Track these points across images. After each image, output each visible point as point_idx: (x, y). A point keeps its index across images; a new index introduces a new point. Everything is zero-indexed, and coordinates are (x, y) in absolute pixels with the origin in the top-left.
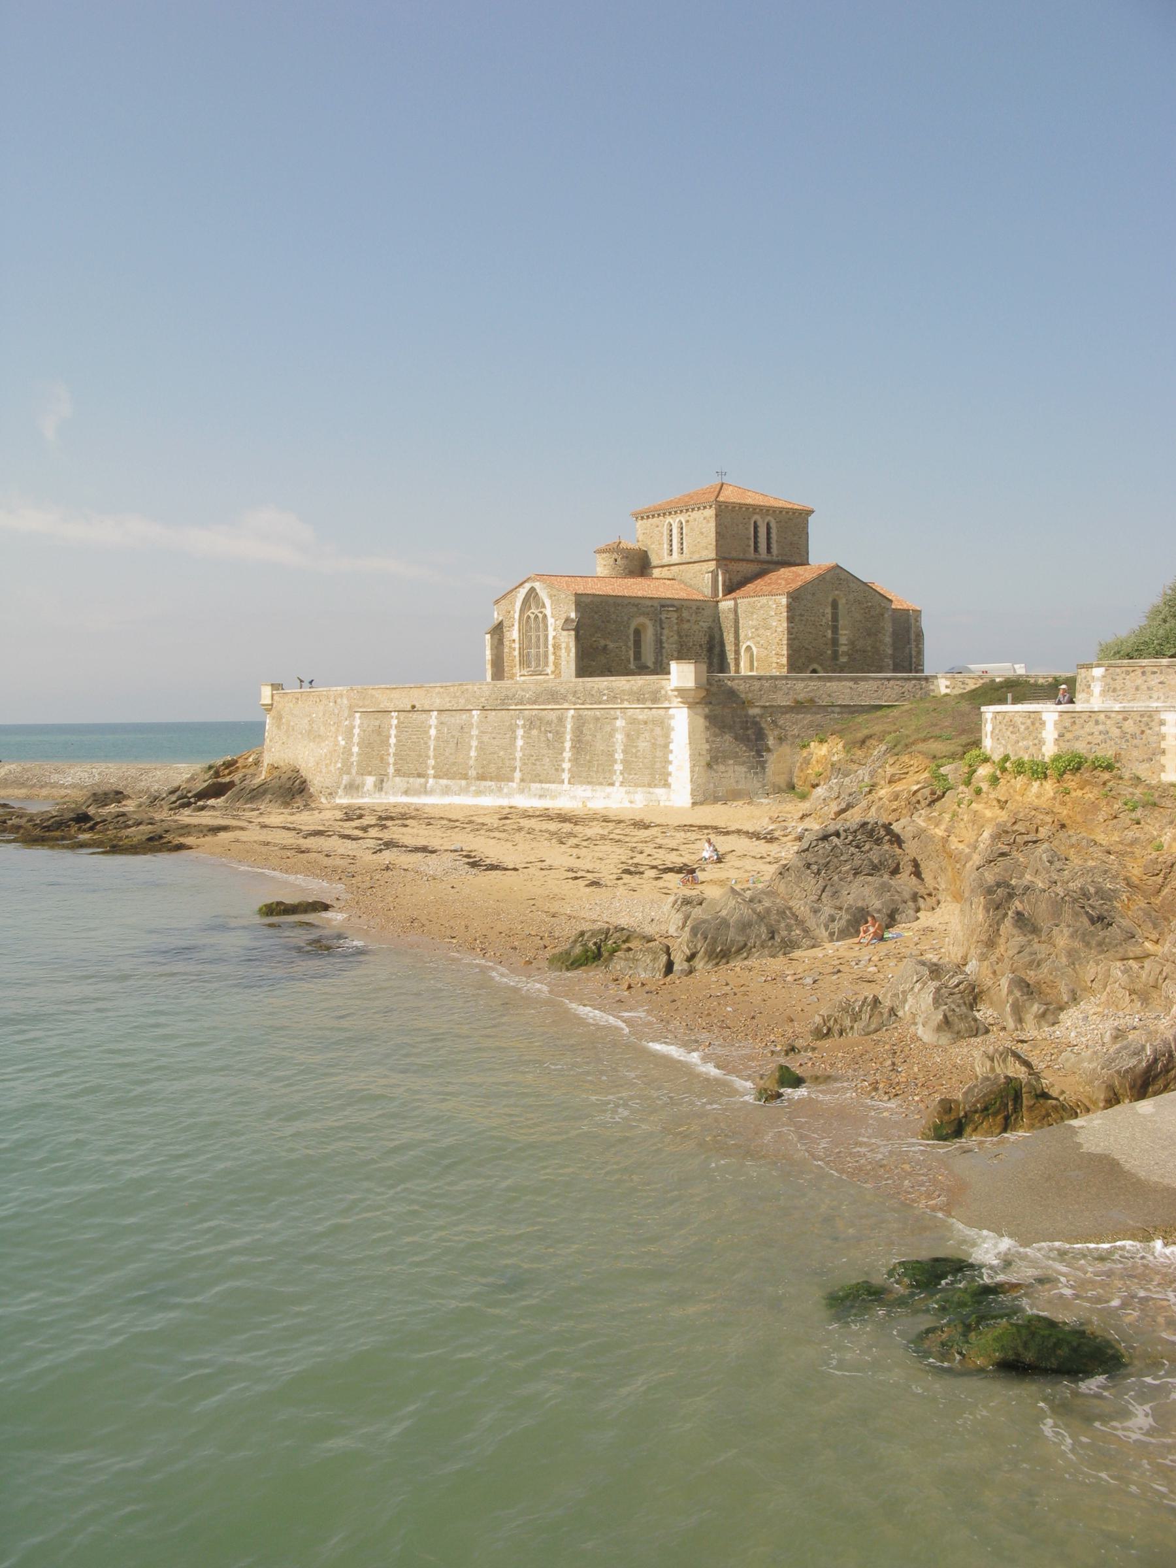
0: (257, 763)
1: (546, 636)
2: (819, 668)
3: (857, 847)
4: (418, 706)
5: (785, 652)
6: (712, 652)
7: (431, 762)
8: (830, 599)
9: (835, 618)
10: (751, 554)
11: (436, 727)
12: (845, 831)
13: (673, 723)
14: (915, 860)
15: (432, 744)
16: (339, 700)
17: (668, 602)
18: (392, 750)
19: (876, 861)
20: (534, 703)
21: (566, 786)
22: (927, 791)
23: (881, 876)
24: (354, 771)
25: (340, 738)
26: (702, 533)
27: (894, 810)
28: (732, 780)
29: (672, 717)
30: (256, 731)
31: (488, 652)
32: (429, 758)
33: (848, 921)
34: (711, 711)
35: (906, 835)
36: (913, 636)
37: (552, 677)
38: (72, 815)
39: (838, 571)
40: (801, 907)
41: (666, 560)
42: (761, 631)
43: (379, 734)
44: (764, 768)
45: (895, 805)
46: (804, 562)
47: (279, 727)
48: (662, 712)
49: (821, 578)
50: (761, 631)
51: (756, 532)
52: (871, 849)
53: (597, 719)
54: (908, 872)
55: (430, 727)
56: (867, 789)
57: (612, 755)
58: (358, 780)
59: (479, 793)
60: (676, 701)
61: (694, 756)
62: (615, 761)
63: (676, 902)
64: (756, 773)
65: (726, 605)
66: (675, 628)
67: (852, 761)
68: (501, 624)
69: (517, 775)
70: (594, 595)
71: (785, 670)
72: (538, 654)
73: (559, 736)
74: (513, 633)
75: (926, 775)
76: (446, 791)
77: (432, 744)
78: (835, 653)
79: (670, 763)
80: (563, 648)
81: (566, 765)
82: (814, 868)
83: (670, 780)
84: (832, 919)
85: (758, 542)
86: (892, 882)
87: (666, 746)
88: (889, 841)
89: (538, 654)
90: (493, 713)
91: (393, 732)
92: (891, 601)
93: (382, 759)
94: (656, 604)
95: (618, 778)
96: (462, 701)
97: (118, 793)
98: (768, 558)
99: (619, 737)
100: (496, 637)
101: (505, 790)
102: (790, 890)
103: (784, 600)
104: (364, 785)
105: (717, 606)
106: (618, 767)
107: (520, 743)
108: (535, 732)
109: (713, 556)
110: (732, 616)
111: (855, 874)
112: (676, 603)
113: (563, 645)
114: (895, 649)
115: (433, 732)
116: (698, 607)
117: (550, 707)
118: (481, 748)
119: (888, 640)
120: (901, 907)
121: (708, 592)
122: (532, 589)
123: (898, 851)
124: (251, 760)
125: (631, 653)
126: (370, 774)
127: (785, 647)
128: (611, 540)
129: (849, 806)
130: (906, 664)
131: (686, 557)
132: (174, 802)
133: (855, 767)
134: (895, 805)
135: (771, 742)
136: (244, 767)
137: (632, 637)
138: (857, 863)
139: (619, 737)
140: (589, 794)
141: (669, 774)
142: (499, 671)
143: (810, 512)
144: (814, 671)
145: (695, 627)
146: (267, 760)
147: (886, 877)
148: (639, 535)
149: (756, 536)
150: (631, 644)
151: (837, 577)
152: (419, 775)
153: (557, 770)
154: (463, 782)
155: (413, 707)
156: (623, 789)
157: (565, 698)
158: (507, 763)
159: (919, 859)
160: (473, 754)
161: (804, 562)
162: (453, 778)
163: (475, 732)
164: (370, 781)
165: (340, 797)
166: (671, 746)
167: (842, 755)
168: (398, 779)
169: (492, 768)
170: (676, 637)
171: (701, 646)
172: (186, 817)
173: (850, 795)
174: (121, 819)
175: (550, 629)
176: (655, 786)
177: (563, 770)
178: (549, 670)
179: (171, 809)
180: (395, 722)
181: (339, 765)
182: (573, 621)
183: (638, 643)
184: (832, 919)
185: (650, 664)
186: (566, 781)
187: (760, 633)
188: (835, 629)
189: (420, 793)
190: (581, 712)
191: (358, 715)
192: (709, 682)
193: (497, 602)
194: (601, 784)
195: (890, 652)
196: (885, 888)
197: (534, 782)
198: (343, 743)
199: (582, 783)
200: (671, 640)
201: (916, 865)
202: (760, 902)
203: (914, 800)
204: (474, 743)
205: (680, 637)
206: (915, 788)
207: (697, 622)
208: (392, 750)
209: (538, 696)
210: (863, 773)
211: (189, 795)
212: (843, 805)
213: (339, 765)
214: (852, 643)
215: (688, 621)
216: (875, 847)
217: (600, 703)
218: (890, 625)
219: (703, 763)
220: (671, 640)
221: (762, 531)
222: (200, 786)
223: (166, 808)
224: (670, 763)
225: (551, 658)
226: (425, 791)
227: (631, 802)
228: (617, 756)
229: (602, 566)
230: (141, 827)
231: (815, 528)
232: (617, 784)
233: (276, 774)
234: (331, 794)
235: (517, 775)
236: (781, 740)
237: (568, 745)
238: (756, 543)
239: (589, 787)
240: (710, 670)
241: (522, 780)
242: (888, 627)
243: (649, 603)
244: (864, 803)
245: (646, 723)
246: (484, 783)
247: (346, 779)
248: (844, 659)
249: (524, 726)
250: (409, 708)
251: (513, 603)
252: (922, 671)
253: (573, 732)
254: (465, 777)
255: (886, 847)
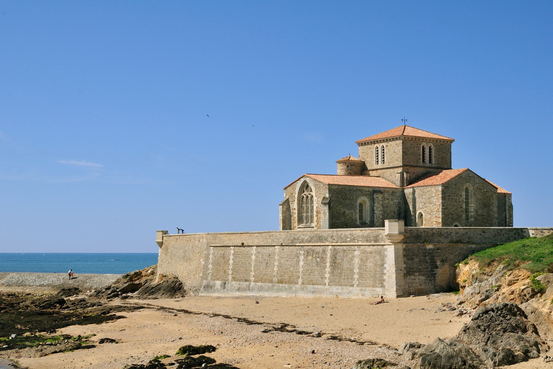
0: (153, 273)
1: (312, 207)
2: (459, 225)
3: (504, 317)
4: (245, 244)
5: (441, 216)
6: (404, 214)
7: (253, 274)
8: (465, 187)
9: (467, 198)
10: (421, 164)
11: (255, 255)
12: (496, 308)
13: (386, 253)
14: (533, 325)
15: (253, 264)
16: (201, 240)
17: (378, 189)
18: (230, 267)
19: (514, 325)
20: (310, 242)
21: (327, 287)
22: (530, 290)
23: (518, 333)
24: (209, 278)
25: (202, 260)
26: (395, 152)
27: (511, 300)
28: (418, 284)
29: (386, 250)
30: (154, 258)
31: (281, 215)
32: (251, 271)
33: (503, 356)
34: (406, 246)
35: (527, 311)
36: (507, 208)
37: (316, 228)
38: (56, 300)
39: (469, 172)
40: (477, 348)
41: (375, 166)
42: (427, 205)
43: (224, 258)
44: (435, 277)
45: (512, 297)
46: (450, 168)
47: (166, 254)
48: (380, 247)
49: (459, 176)
50: (427, 205)
51: (423, 151)
52: (510, 318)
53: (344, 251)
54: (531, 331)
55: (252, 254)
56: (496, 288)
57: (352, 270)
58: (212, 283)
59: (280, 290)
60: (387, 242)
61: (398, 270)
62: (354, 273)
63: (406, 346)
64: (430, 280)
65: (408, 191)
66: (381, 203)
67: (483, 274)
68: (288, 199)
69: (300, 281)
70: (338, 185)
71: (441, 225)
72: (307, 217)
73: (323, 260)
74: (294, 206)
75: (528, 281)
76: (261, 289)
77: (253, 264)
78: (467, 216)
79: (385, 274)
80: (321, 214)
81: (327, 276)
82: (482, 328)
83: (385, 284)
84: (495, 355)
85: (424, 159)
86: (524, 336)
87: (382, 265)
88: (520, 314)
89: (307, 217)
90: (287, 247)
91: (231, 257)
92: (497, 188)
93: (225, 272)
94: (371, 190)
95: (356, 282)
96: (270, 241)
97: (76, 289)
98: (430, 165)
99: (356, 260)
100: (285, 207)
101: (293, 289)
102: (470, 340)
103: (440, 188)
104: (214, 285)
105: (403, 191)
106: (356, 276)
107: (301, 263)
108: (310, 258)
109: (401, 164)
110: (411, 197)
111: (504, 332)
112: (381, 190)
113: (322, 212)
114: (499, 214)
115: (253, 257)
116: (392, 192)
117: (311, 244)
118: (280, 266)
119: (495, 209)
120: (530, 349)
121: (398, 183)
122: (305, 182)
123: (525, 320)
124: (149, 272)
125: (358, 216)
126: (218, 279)
127: (441, 213)
128: (343, 156)
129: (487, 297)
130: (503, 222)
131: (386, 165)
132: (110, 294)
133: (486, 277)
134: (512, 297)
135: (438, 263)
136: (145, 276)
137: (358, 208)
138: (504, 325)
139: (356, 260)
140: (340, 291)
141: (384, 280)
142: (287, 225)
143: (452, 141)
144: (456, 226)
145: (391, 202)
146: (159, 271)
147: (520, 333)
148: (361, 154)
149: (423, 154)
150: (358, 211)
151: (469, 176)
152: (246, 281)
153: (322, 278)
154: (270, 284)
155: (243, 244)
156: (358, 288)
157: (326, 240)
158: (295, 274)
159: (535, 324)
160: (276, 269)
161: (450, 168)
162: (265, 282)
163: (277, 257)
164: (218, 283)
165: (202, 292)
166: (385, 266)
167: (478, 271)
168: (234, 282)
169: (286, 277)
170: (381, 208)
171: (394, 212)
172: (117, 302)
173: (487, 291)
174: (83, 303)
175: (315, 203)
176: (376, 287)
177: (325, 278)
178: (313, 225)
179: (108, 298)
180: (232, 252)
181: (201, 275)
182: (327, 199)
183: (361, 211)
184: (495, 355)
185: (368, 222)
186: (327, 284)
187: (429, 204)
188: (467, 203)
189: (246, 290)
190: (335, 247)
191: (212, 248)
192: (406, 231)
193: (286, 188)
194: (347, 285)
195: (496, 216)
196: (520, 339)
197: (309, 284)
198: (203, 263)
199: (336, 285)
200: (379, 209)
201: (535, 327)
202: (455, 345)
203: (523, 294)
204: (276, 263)
205: (384, 207)
206: (523, 287)
207: (392, 200)
208: (230, 267)
209: (312, 238)
210: (492, 280)
211: (118, 290)
212: (483, 297)
213: (201, 275)
214: (476, 211)
215: (388, 199)
216: (513, 317)
217: (346, 242)
218: (496, 201)
219: (402, 274)
220: (379, 209)
221: (427, 151)
222: (122, 286)
223: (105, 297)
224: (385, 274)
225: (315, 218)
226: (249, 289)
227: (363, 295)
228: (355, 271)
229: (340, 169)
230: (95, 307)
231: (455, 149)
232: (355, 286)
233: (164, 279)
234: (196, 290)
235: (300, 281)
236: (443, 261)
237: (328, 264)
238: (423, 157)
239: (340, 287)
240: (406, 225)
241: (303, 283)
242: (495, 203)
243: (367, 189)
244: (495, 296)
245: (371, 253)
246: (281, 285)
247: (205, 282)
248: (473, 220)
249: (304, 254)
250: (240, 244)
251: (294, 189)
252: (512, 226)
253: (331, 258)
254: (271, 282)
255: (518, 318)
